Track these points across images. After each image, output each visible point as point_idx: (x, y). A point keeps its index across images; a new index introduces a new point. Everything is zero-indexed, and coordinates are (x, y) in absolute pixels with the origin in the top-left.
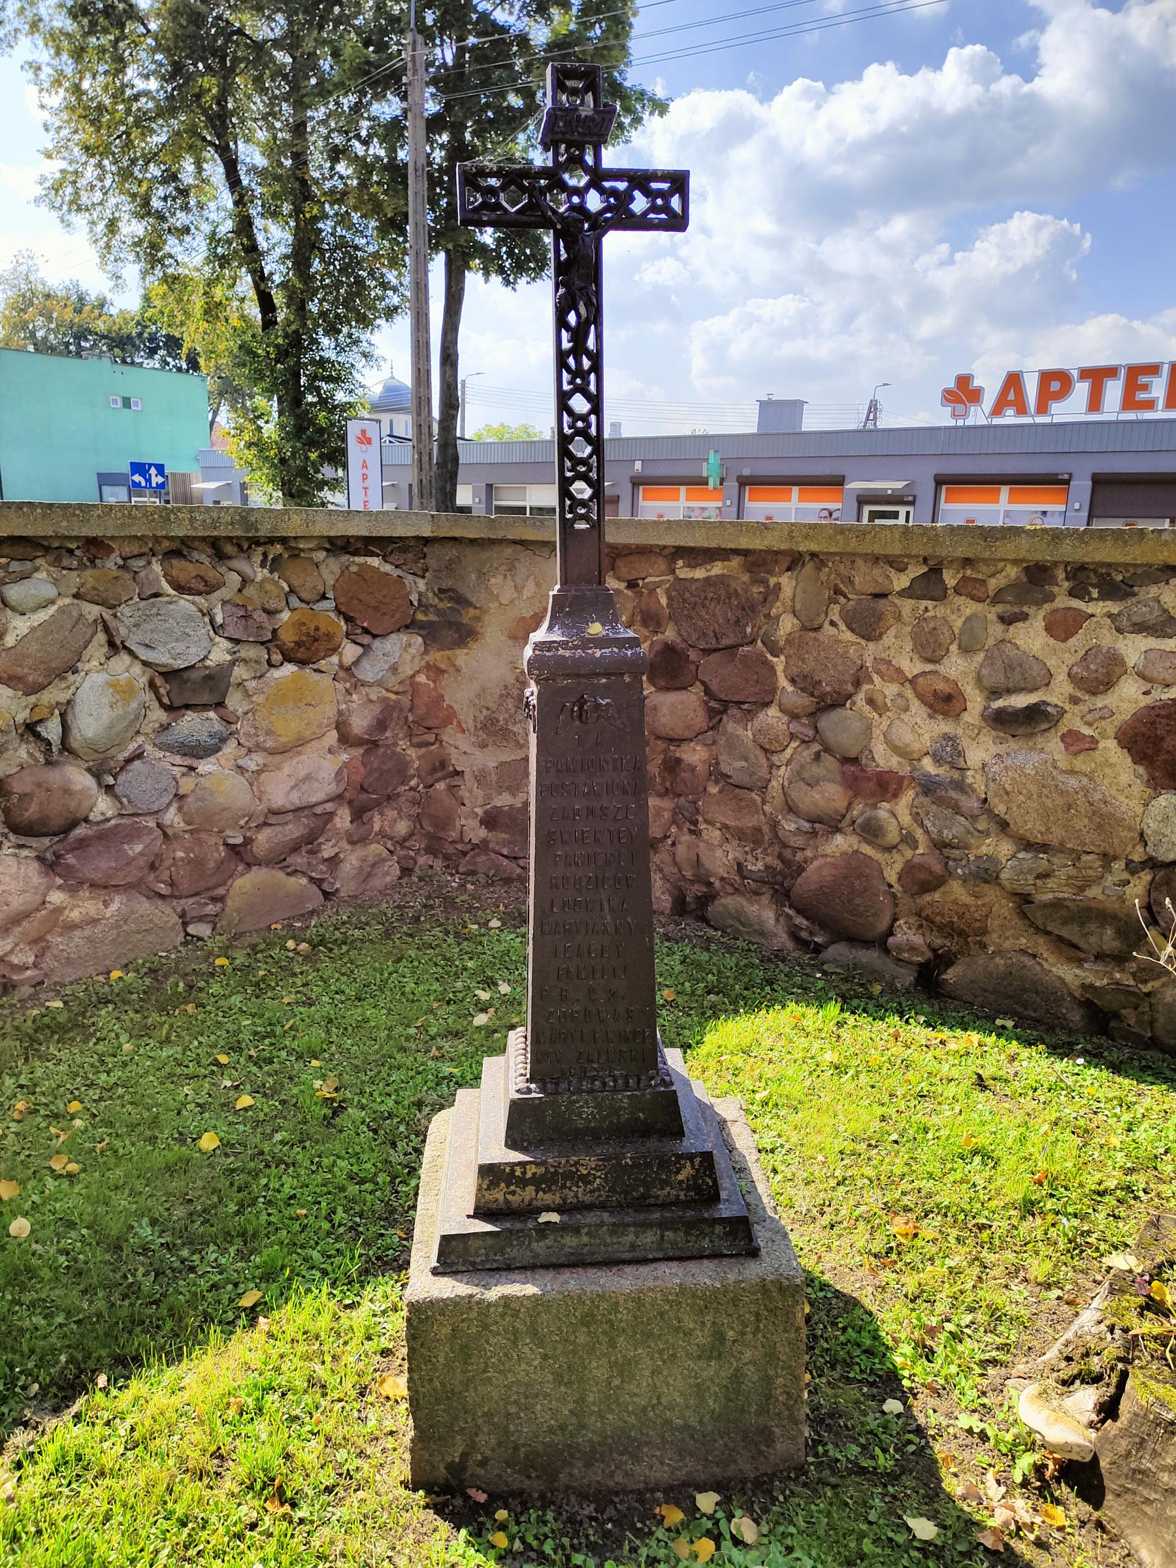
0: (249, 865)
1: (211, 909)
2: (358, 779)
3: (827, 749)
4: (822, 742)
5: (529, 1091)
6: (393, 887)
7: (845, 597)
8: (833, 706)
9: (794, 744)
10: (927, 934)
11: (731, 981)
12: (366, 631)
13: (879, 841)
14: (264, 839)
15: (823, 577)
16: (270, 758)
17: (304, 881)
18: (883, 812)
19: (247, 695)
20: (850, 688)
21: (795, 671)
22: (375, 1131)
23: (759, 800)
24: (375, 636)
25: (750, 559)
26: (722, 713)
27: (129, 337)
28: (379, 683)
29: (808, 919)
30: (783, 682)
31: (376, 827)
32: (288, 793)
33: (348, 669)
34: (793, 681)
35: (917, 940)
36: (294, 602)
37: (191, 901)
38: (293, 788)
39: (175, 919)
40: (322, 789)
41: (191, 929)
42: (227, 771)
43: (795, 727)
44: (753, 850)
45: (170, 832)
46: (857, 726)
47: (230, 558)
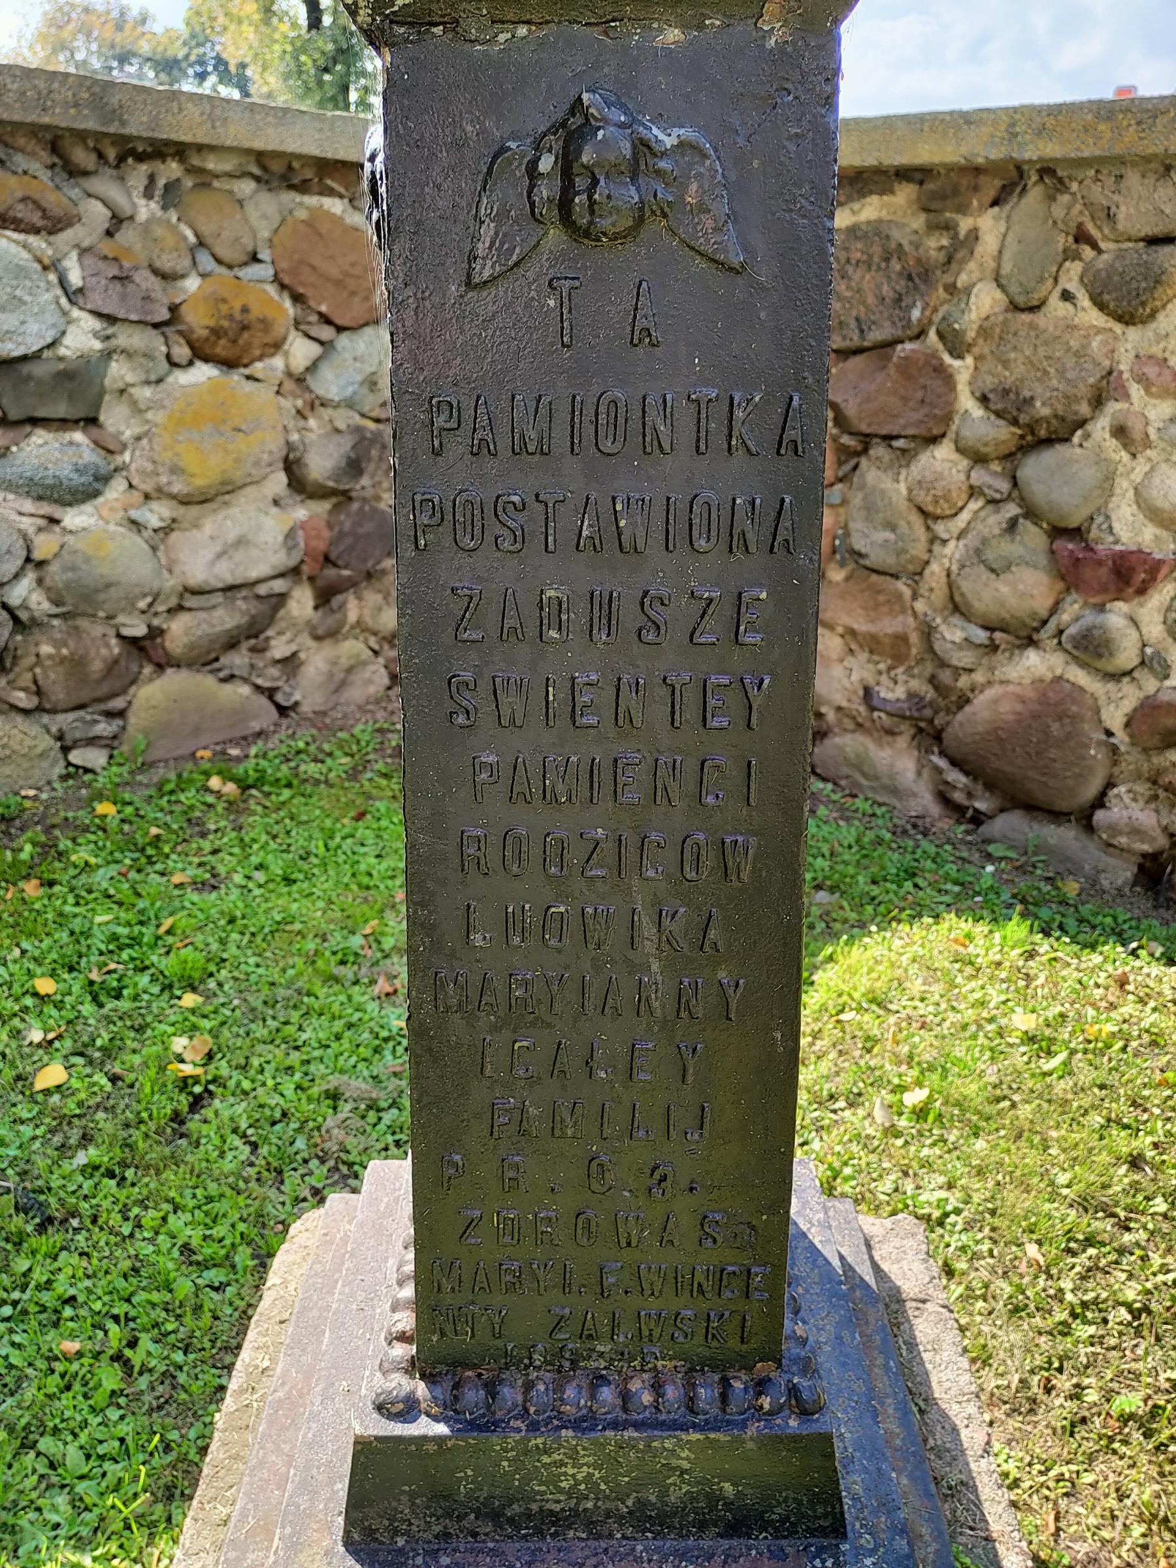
0: (160, 667)
1: (104, 728)
2: (321, 546)
3: (1031, 513)
4: (1023, 501)
5: (408, 1410)
6: (377, 702)
7: (1094, 246)
8: (1048, 442)
9: (974, 505)
10: (1164, 812)
11: (851, 870)
12: (326, 320)
13: (1100, 664)
14: (180, 632)
15: (1058, 211)
16: (182, 510)
17: (245, 690)
18: (1116, 616)
19: (138, 410)
20: (1084, 409)
21: (989, 382)
22: (255, 1146)
23: (907, 593)
24: (340, 329)
25: (930, 186)
26: (858, 454)
27: (176, 62)
28: (349, 404)
29: (967, 774)
30: (966, 402)
31: (352, 617)
32: (212, 563)
33: (300, 380)
34: (984, 400)
35: (1146, 818)
36: (206, 261)
37: (71, 716)
38: (219, 556)
39: (47, 742)
40: (266, 556)
41: (75, 757)
42: (112, 527)
43: (979, 476)
44: (890, 669)
45: (24, 616)
46: (1089, 475)
47: (86, 173)
